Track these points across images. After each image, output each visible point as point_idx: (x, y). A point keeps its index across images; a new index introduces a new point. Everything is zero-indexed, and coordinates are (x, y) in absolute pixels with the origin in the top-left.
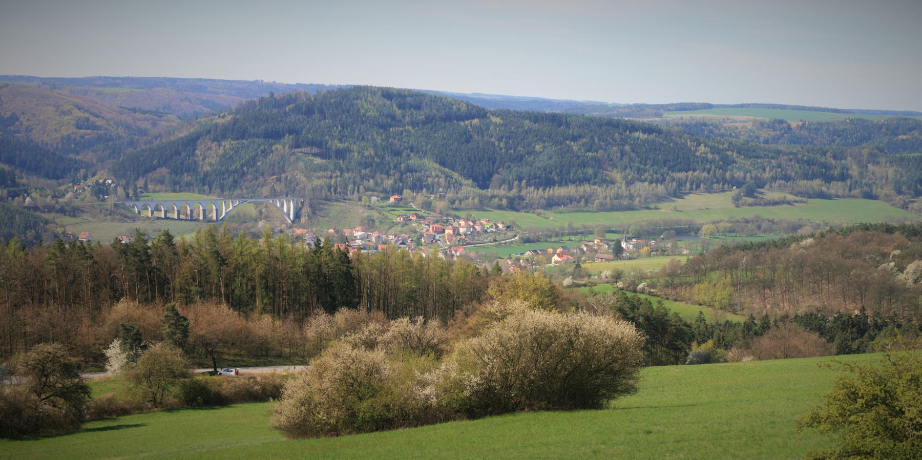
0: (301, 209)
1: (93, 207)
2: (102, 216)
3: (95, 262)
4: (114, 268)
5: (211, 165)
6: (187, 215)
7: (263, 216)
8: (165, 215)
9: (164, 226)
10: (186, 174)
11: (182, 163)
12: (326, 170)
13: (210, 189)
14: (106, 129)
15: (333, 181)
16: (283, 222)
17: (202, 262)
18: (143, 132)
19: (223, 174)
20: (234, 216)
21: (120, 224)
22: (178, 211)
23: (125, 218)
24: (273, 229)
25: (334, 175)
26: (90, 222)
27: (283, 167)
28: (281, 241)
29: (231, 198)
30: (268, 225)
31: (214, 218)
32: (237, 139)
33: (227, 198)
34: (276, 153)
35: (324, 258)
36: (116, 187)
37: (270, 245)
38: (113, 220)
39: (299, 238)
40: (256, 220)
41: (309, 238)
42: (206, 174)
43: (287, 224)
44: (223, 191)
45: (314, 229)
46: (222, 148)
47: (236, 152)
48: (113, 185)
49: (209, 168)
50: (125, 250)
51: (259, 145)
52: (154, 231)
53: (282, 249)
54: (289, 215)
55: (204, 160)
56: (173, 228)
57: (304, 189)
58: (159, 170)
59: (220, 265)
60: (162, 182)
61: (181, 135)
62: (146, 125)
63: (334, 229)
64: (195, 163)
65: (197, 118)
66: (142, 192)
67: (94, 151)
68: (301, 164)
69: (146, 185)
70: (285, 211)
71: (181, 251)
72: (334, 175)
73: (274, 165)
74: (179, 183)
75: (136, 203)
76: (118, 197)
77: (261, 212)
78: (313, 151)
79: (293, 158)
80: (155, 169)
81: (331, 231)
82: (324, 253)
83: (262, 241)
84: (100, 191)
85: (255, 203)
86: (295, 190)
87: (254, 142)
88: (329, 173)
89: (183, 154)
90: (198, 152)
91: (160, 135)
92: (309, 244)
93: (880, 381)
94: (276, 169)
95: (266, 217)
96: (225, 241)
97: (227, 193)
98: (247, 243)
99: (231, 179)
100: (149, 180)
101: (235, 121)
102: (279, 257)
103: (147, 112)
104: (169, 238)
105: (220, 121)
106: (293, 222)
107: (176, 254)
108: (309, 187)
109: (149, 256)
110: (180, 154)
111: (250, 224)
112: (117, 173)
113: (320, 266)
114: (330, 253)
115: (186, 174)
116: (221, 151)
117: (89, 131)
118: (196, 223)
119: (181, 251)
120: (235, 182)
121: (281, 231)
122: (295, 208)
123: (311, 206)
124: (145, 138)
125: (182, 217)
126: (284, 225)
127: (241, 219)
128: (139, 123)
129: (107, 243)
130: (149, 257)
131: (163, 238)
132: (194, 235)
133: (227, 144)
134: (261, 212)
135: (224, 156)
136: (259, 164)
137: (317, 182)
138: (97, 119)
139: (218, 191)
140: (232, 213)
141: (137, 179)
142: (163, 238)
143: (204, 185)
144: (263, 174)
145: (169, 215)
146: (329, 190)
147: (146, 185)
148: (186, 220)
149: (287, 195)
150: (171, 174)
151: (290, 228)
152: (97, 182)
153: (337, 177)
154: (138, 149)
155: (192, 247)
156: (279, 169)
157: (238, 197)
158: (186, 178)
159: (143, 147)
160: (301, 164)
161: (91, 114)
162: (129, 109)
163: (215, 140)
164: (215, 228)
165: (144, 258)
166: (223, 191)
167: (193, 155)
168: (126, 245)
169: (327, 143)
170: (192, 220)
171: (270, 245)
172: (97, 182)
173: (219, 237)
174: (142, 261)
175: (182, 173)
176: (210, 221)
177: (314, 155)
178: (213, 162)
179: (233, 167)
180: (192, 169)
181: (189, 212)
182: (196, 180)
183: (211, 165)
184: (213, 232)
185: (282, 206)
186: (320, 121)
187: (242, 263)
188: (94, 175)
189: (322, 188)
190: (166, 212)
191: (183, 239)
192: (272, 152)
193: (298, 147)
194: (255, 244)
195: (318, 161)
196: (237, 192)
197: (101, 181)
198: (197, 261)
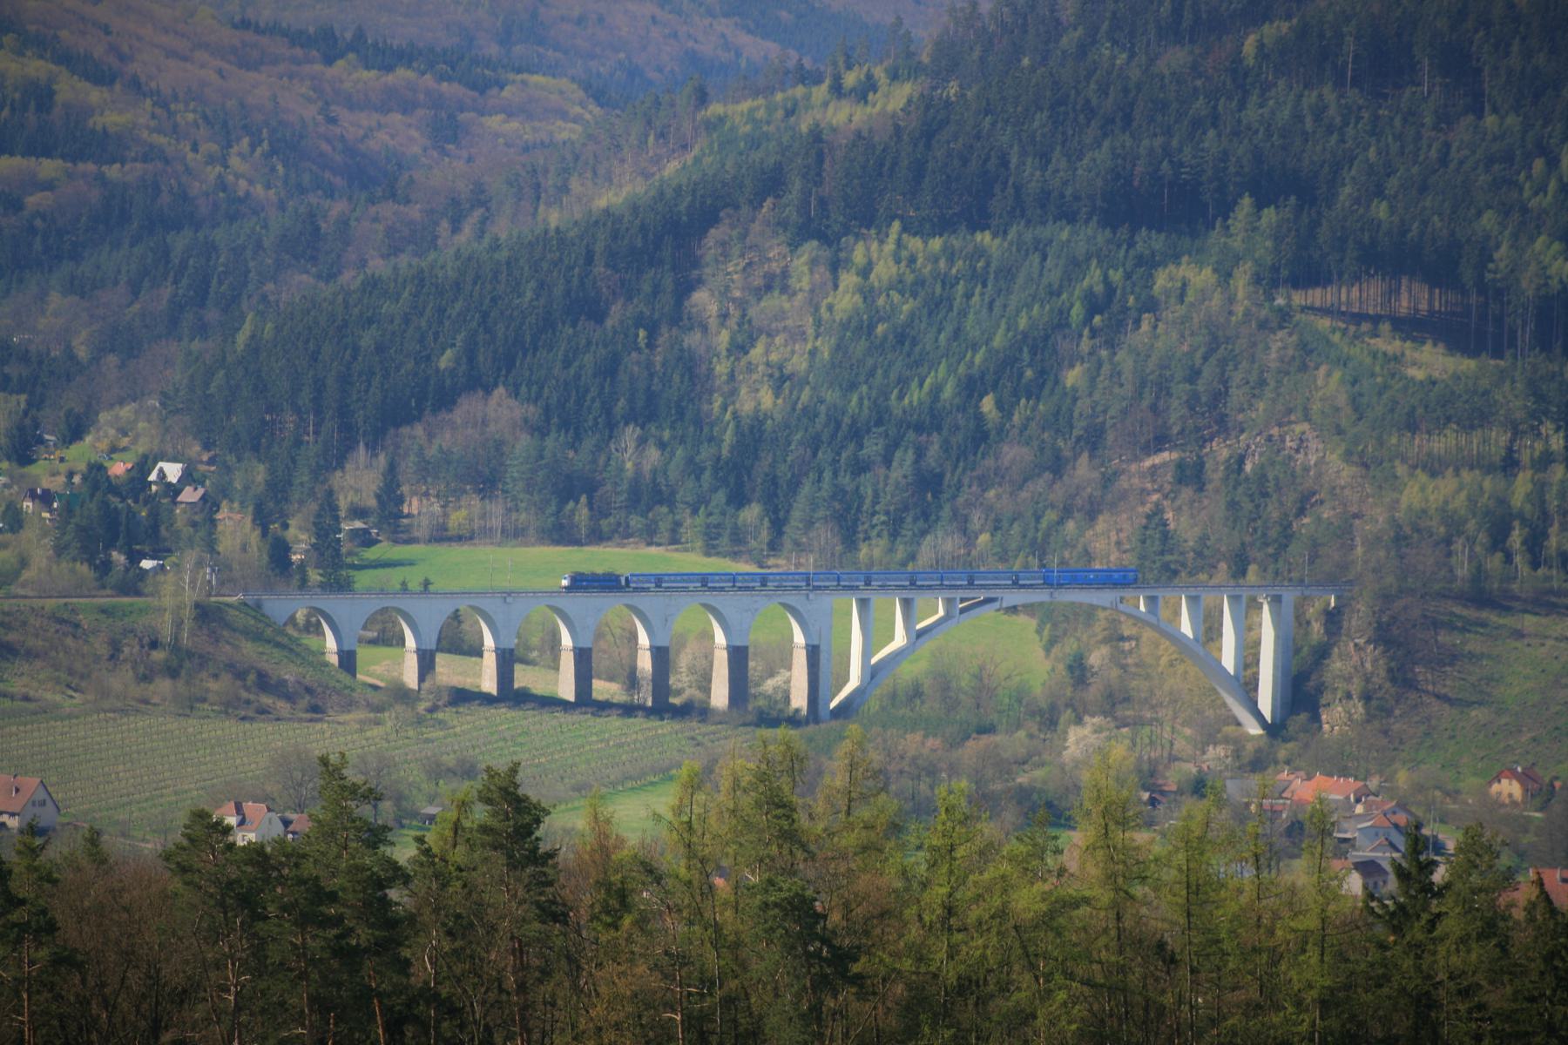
0: (1322, 653)
1: (67, 623)
2: (121, 680)
3: (65, 960)
4: (183, 996)
5: (781, 379)
6: (632, 681)
7: (1094, 692)
8: (505, 675)
9: (494, 740)
10: (630, 434)
11: (610, 369)
12: (1477, 418)
13: (778, 526)
14: (150, 154)
15: (1522, 485)
16: (1216, 729)
17: (712, 961)
18: (373, 178)
19: (857, 434)
20: (916, 692)
21: (230, 728)
22: (583, 657)
23: (259, 692)
24: (1149, 777)
25: (1529, 449)
26: (48, 711)
27: (1219, 396)
28: (1196, 845)
29: (913, 584)
30: (1119, 751)
31: (799, 700)
32: (943, 226)
33: (864, 583)
34: (1175, 311)
35: (1452, 956)
36: (209, 504)
37: (1124, 871)
38: (190, 705)
39: (1312, 831)
40: (1049, 719)
41: (1366, 829)
42: (753, 436)
43: (1238, 743)
44: (850, 539)
45: (1403, 778)
46: (848, 279)
47: (936, 306)
48: (190, 495)
49: (767, 399)
50: (247, 889)
51: (1076, 266)
52: (437, 772)
53: (1197, 892)
54: (1247, 688)
55: (739, 348)
56: (541, 753)
57: (1344, 533)
58: (468, 406)
59: (822, 984)
60: (487, 482)
61: (608, 199)
62: (398, 135)
63: (1526, 778)
64: (692, 368)
65: (702, 98)
66: (366, 540)
67: (75, 287)
68: (1329, 384)
69: (390, 497)
70: (1228, 661)
71: (586, 901)
72: (1529, 449)
73: (1163, 389)
74: (591, 487)
75: (329, 603)
76: (222, 567)
77: (1079, 670)
78: (1404, 305)
79: (1279, 345)
80: (446, 400)
81: (1509, 788)
82: (1452, 925)
83: (1075, 844)
84: (117, 526)
85: (1045, 614)
86: (1287, 535)
87: (1042, 248)
88: (1498, 439)
89: (617, 313)
90: (704, 301)
91: (480, 197)
92: (1368, 868)
93: (444, 153)
94: (1176, 413)
95: (1114, 703)
96: (850, 840)
97: (872, 551)
98: (987, 853)
99: (904, 463)
100: (408, 466)
101: (932, 120)
102: (1173, 943)
103: (405, 56)
104: (515, 817)
105: (843, 116)
106: (1274, 730)
107: (554, 913)
108: (1376, 519)
109: (392, 924)
110: (599, 316)
111: (1012, 742)
112: (232, 418)
113: (1424, 1003)
114: (1492, 927)
115: (630, 434)
116: (845, 300)
117: (49, 167)
118: (693, 726)
119: (586, 901)
120: (928, 484)
121: (1199, 787)
122: (1288, 648)
123: (1384, 636)
124: (387, 210)
125: (603, 689)
126: (1216, 754)
127: (957, 705)
128: (353, 124)
129: (145, 841)
130: (394, 931)
131: (480, 814)
132: (664, 800)
133: (881, 255)
134: (1079, 670)
135: (860, 326)
136: (1073, 377)
137: (1418, 494)
138: (95, 95)
139: (825, 535)
140: (909, 671)
141: (337, 458)
142: (480, 814)
143: (738, 499)
144: (1093, 440)
145: (524, 678)
146: (1498, 539)
147: (390, 497)
148: (628, 710)
149: (1240, 571)
150: (540, 431)
151: (1258, 763)
152: (96, 471)
153: (1545, 461)
154: (350, 278)
155: (651, 872)
156: (1189, 410)
157: (941, 578)
158: (634, 455)
159: (378, 266)
160: (1329, 384)
161: (66, 59)
162: (297, 38)
163: (807, 229)
164: (794, 762)
165: (363, 935)
166: (850, 539)
167: (679, 317)
168: (257, 854)
169: (1485, 257)
170: (662, 708)
171: (1124, 871)
172: (96, 471)
173: (816, 814)
174: (348, 955)
175: (611, 428)
176: (774, 716)
177: (1412, 327)
178: (799, 364)
179: (916, 396)
180: (674, 402)
181: (645, 663)
182: (694, 469)
183: (781, 379)
184: (784, 783)
185: (1210, 631)
186: (1445, 120)
187: (951, 975)
188: (75, 432)
189: (1455, 526)
190: (507, 661)
191: (601, 825)
192: (1151, 306)
193: (1308, 275)
194: (1029, 867)
195: (1431, 362)
196: (941, 543)
197: (118, 468)
198: (683, 960)
